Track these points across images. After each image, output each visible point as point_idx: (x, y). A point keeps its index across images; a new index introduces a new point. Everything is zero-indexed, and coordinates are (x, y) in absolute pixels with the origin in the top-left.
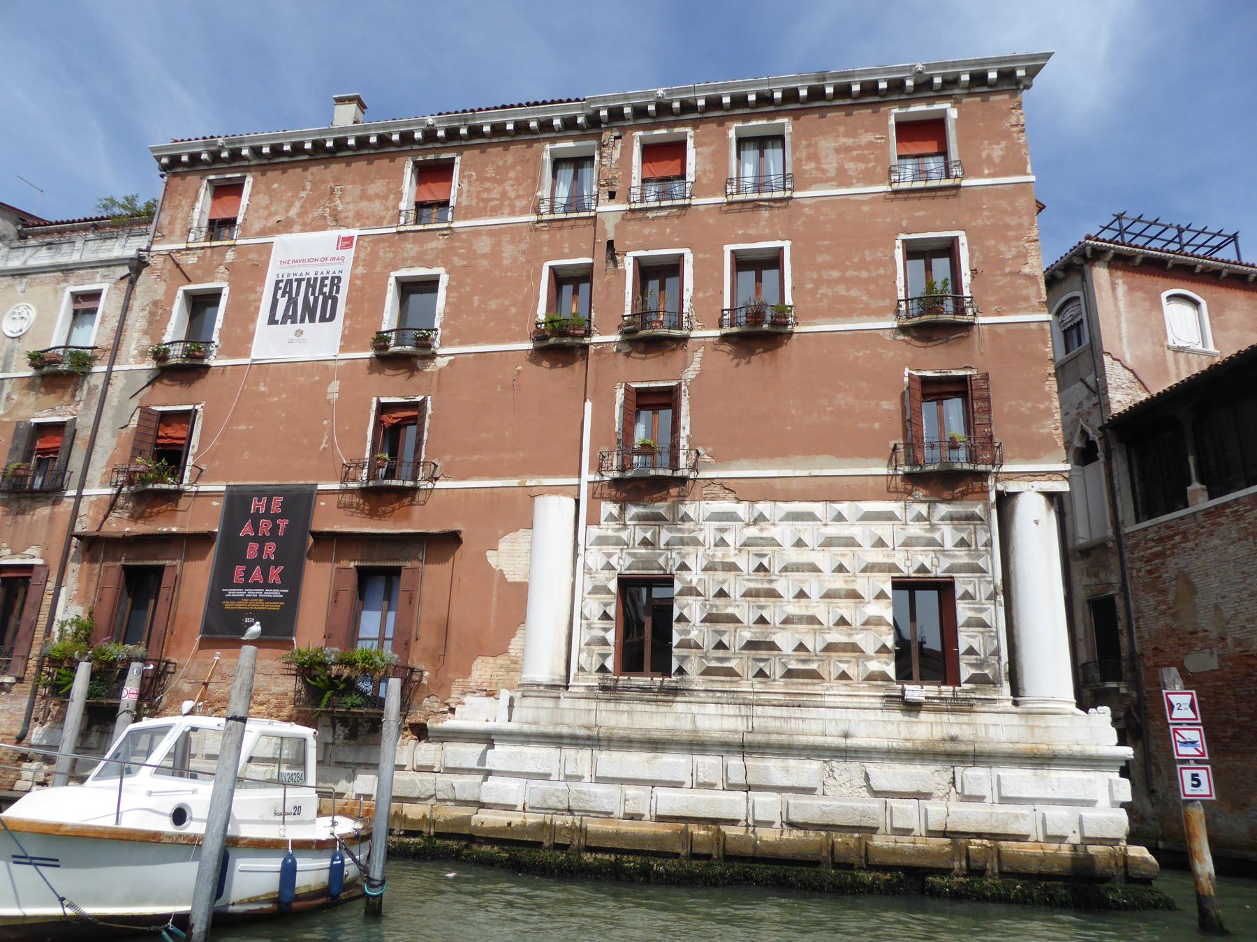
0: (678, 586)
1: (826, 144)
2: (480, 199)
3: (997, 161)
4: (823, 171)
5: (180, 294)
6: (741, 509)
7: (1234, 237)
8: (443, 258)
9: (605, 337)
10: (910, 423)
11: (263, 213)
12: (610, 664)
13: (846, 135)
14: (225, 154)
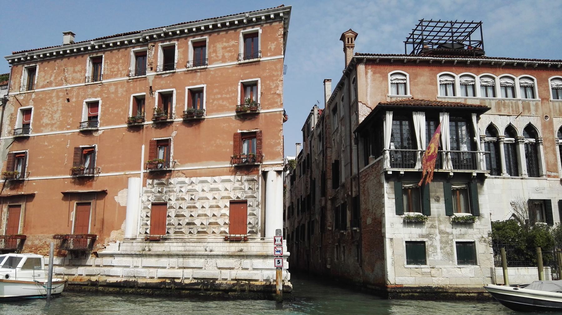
0: (168, 206)
1: (219, 46)
2: (111, 71)
3: (273, 50)
4: (218, 57)
5: (19, 110)
6: (187, 180)
7: (480, 23)
8: (100, 94)
9: (148, 122)
10: (237, 148)
11: (43, 79)
12: (148, 231)
13: (226, 42)
14: (28, 58)
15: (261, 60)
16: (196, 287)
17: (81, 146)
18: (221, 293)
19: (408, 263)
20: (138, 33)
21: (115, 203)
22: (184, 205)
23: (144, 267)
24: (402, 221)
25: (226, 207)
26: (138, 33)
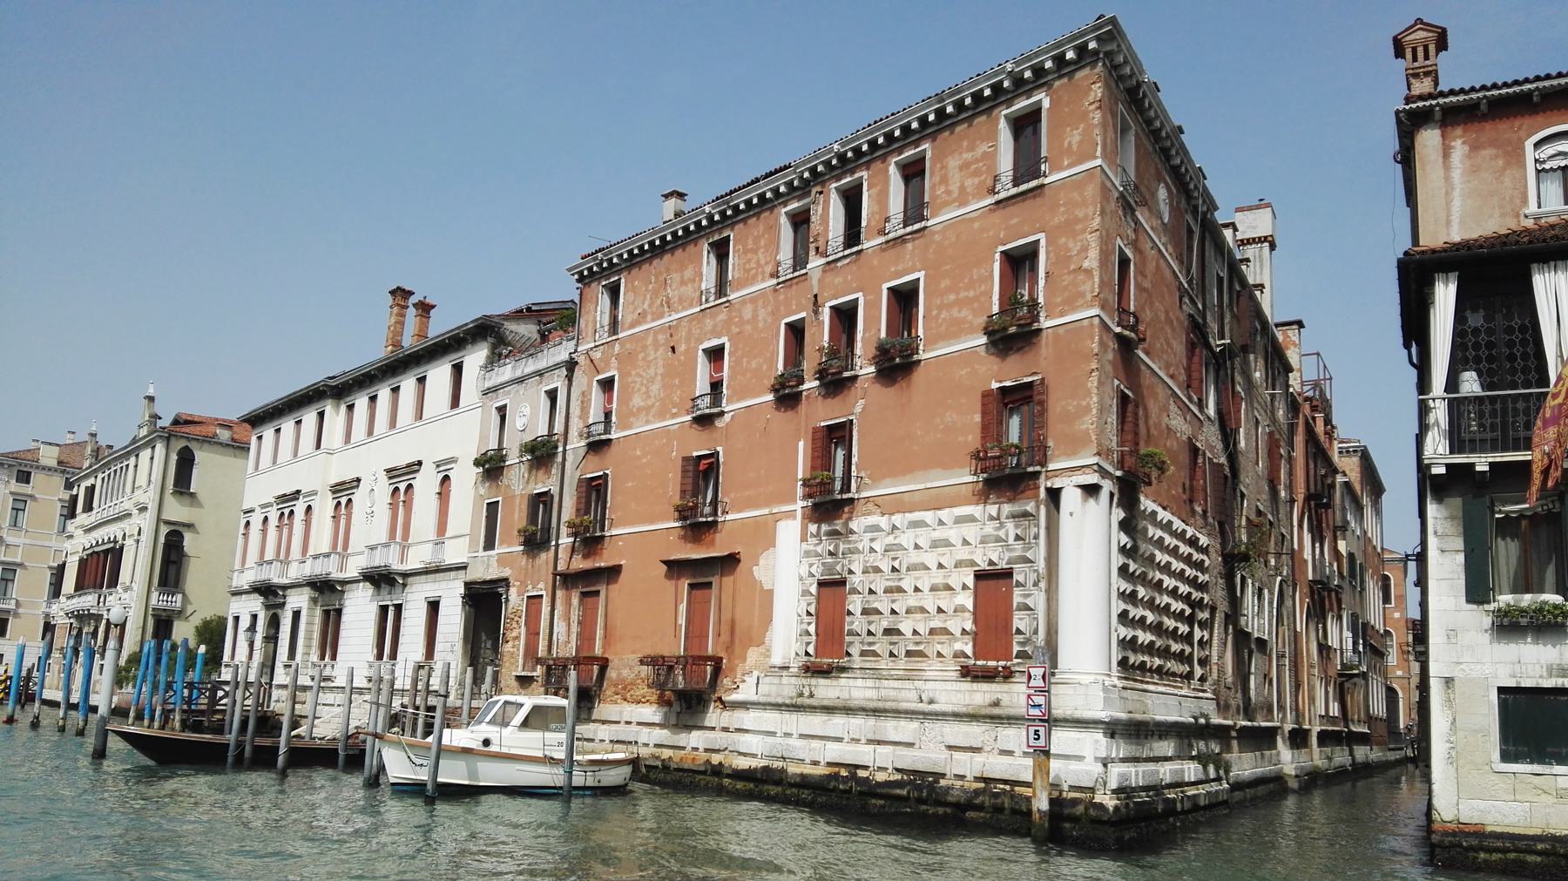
1: (953, 163)
3: (1075, 147)
4: (948, 192)
6: (883, 522)
8: (726, 328)
10: (992, 429)
12: (811, 650)
15: (1047, 181)
16: (898, 791)
17: (695, 454)
18: (948, 810)
19: (1506, 757)
20: (786, 167)
21: (754, 583)
22: (880, 585)
23: (802, 736)
24: (1487, 621)
25: (965, 587)
26: (786, 167)
